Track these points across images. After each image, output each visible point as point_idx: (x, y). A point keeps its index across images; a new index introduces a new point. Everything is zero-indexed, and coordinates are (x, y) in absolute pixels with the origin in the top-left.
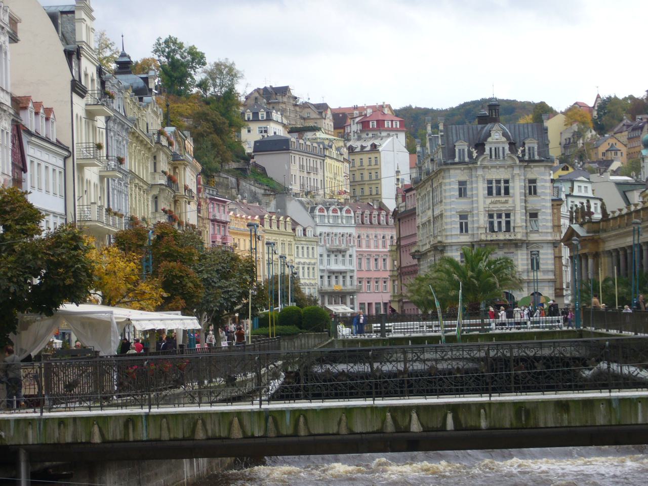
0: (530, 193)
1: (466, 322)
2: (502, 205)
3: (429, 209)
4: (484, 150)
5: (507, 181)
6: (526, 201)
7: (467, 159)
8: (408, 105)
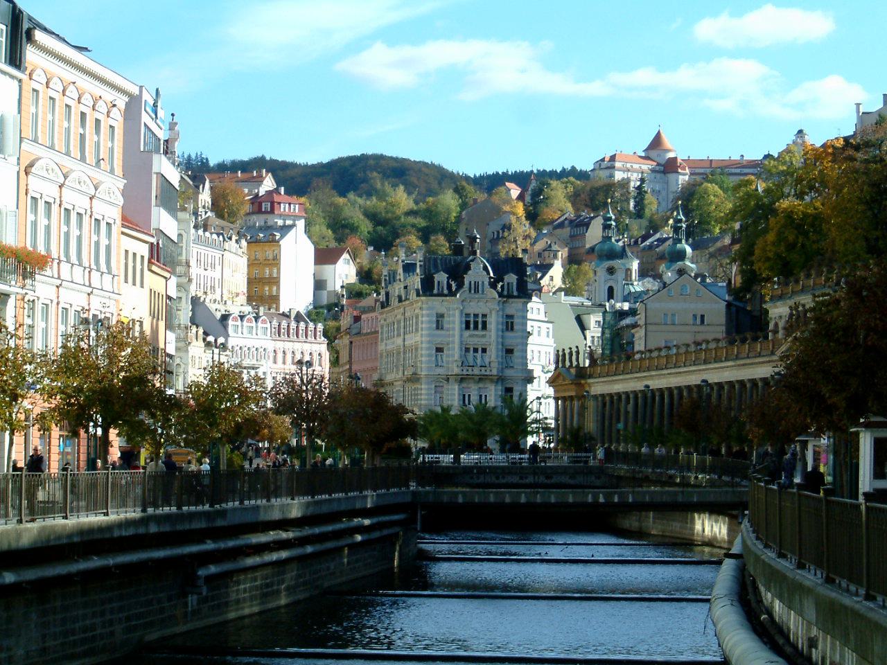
0: (507, 329)
1: (576, 455)
2: (479, 339)
3: (399, 335)
4: (463, 284)
5: (484, 316)
6: (503, 337)
7: (446, 292)
8: (260, 155)
